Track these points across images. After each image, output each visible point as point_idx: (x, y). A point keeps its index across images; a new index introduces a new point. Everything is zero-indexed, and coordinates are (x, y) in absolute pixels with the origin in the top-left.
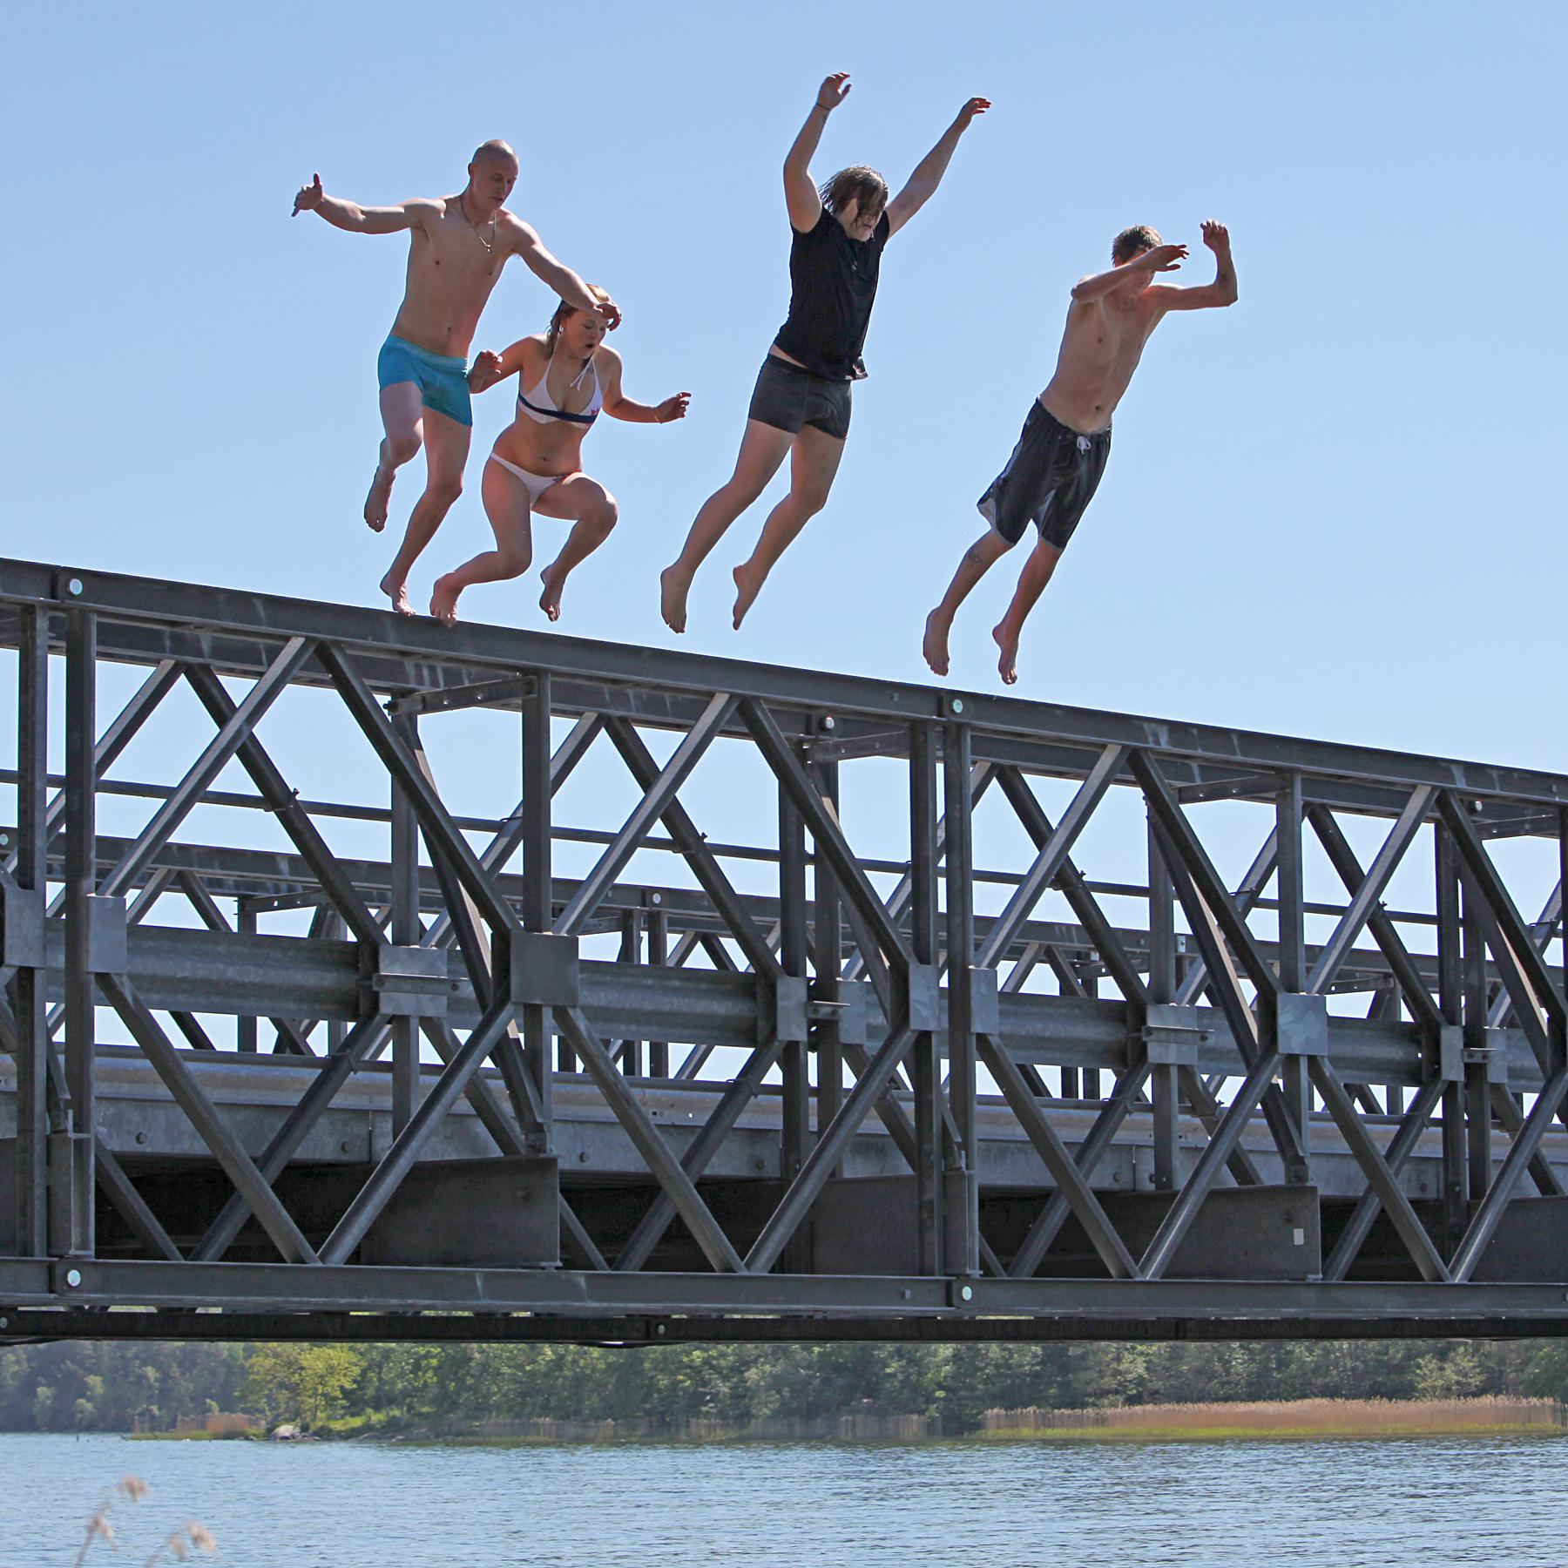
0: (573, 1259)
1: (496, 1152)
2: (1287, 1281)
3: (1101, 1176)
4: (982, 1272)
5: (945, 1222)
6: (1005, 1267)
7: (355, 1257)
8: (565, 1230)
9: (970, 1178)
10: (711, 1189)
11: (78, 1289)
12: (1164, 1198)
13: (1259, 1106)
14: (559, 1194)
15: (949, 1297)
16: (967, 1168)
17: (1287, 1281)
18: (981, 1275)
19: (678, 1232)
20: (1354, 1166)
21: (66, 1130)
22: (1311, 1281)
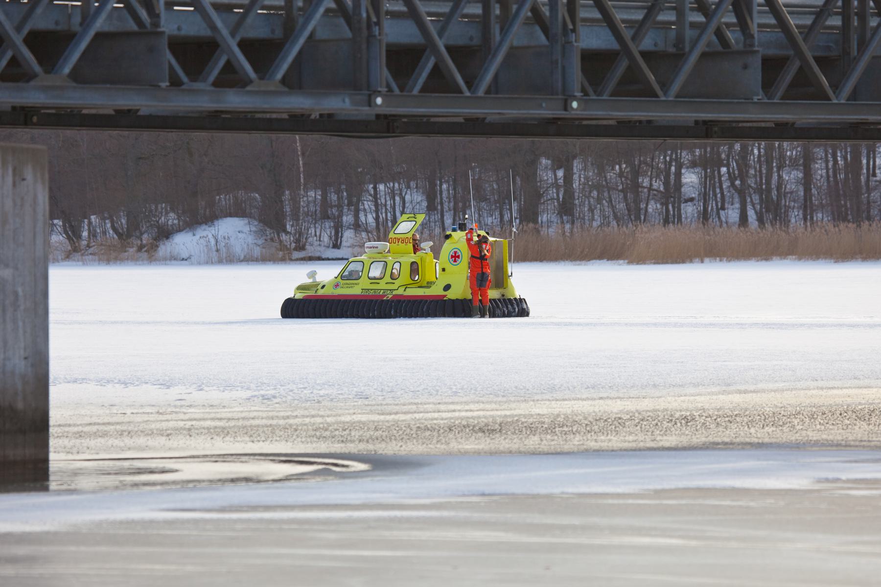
0: (175, 82)
1: (135, 28)
2: (743, 101)
3: (648, 43)
4: (582, 94)
5: (564, 68)
6: (595, 92)
7: (488, 92)
8: (171, 67)
9: (380, 41)
10: (246, 45)
11: (576, 110)
12: (678, 57)
13: (731, 7)
14: (168, 51)
15: (566, 107)
16: (576, 41)
17: (743, 101)
18: (582, 96)
19: (230, 67)
20: (198, 18)
21: (572, 42)
22: (756, 100)
